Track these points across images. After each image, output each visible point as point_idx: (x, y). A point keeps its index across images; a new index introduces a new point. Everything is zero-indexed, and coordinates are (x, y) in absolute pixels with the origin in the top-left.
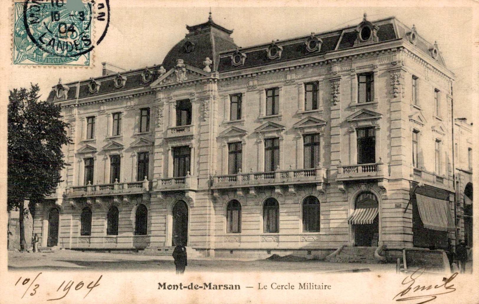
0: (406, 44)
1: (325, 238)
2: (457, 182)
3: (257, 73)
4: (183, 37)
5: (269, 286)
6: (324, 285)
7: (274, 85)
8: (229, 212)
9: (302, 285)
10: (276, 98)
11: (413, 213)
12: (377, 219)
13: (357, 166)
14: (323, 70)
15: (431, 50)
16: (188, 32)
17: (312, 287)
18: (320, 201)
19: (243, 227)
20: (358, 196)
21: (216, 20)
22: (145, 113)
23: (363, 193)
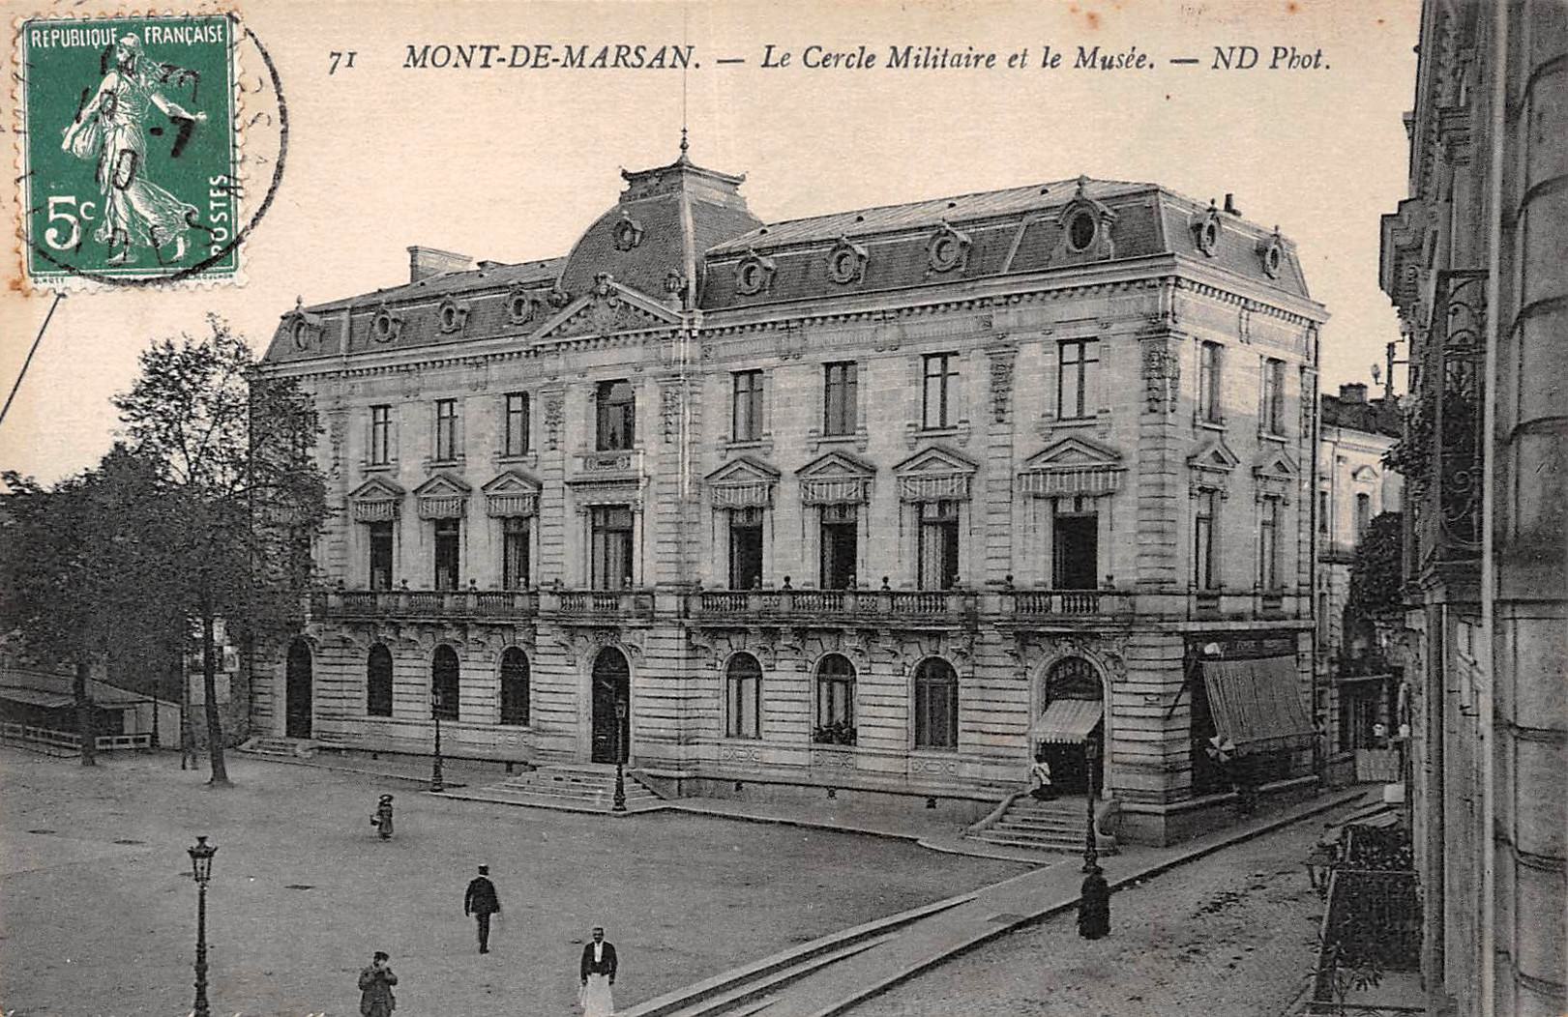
0: (1188, 266)
1: (967, 771)
2: (1323, 494)
3: (802, 320)
4: (613, 201)
5: (796, 59)
6: (973, 54)
7: (844, 356)
8: (733, 683)
9: (901, 51)
10: (849, 389)
11: (1193, 714)
12: (1098, 731)
13: (1050, 594)
14: (968, 321)
15: (1261, 252)
16: (625, 186)
17: (931, 62)
18: (959, 672)
19: (765, 726)
20: (1054, 669)
21: (695, 158)
22: (516, 403)
23: (1063, 661)
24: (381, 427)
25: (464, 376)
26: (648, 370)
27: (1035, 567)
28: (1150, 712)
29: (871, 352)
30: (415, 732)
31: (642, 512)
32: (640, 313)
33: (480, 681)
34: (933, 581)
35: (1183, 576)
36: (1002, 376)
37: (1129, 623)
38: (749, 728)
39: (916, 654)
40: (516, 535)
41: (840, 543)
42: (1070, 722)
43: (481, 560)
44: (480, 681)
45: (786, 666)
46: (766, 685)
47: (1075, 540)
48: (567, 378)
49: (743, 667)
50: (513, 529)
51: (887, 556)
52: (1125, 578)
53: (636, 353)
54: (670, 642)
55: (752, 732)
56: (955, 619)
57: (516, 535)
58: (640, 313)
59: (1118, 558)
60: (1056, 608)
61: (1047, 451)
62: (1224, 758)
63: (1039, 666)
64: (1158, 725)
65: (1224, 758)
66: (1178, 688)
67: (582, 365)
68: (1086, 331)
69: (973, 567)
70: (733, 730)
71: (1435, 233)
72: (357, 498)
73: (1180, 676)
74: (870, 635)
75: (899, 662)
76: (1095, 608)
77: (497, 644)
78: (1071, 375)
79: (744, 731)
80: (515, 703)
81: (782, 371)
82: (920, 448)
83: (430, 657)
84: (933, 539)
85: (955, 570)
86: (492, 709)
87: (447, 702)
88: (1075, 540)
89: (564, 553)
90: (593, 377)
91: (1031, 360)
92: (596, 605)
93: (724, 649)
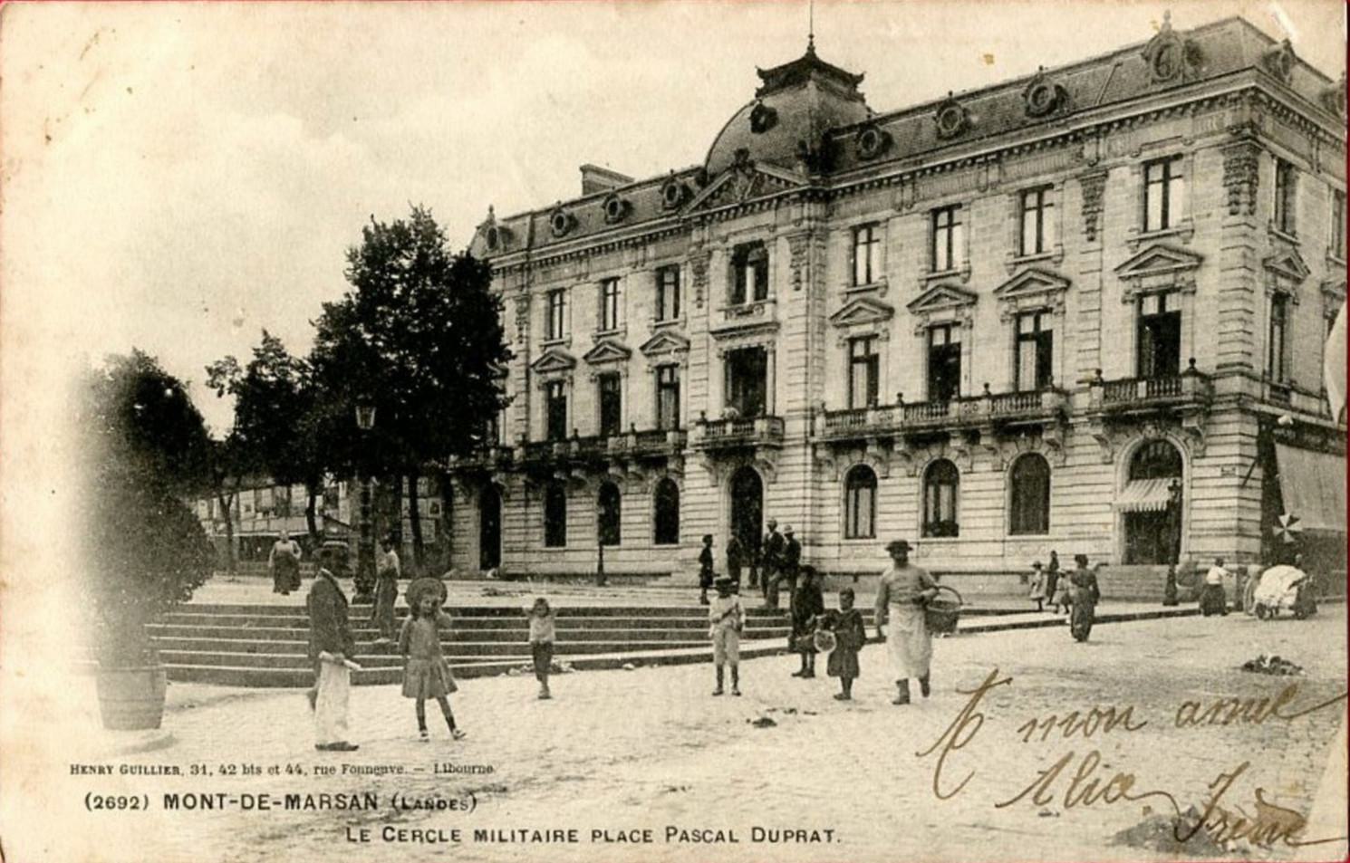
14: (1062, 157)
19: (879, 526)
24: (557, 309)
25: (484, 758)
26: (780, 230)
27: (1120, 362)
28: (1227, 481)
29: (974, 193)
30: (586, 556)
31: (774, 352)
32: (774, 181)
33: (637, 511)
34: (1028, 381)
35: (1259, 367)
36: (1093, 200)
37: (1207, 406)
38: (864, 527)
39: (1012, 451)
40: (668, 387)
41: (943, 367)
42: (1154, 495)
43: (638, 406)
44: (637, 511)
45: (898, 472)
46: (880, 491)
47: (1160, 336)
48: (712, 245)
49: (861, 479)
50: (666, 378)
51: (988, 366)
52: (1206, 364)
53: (768, 218)
54: (797, 461)
55: (868, 533)
56: (1049, 412)
57: (668, 387)
58: (774, 181)
59: (1202, 345)
60: (1142, 393)
61: (1133, 260)
62: (1288, 538)
63: (1127, 444)
64: (1235, 493)
65: (1288, 538)
66: (1251, 462)
67: (724, 233)
68: (1169, 150)
69: (1066, 370)
70: (851, 533)
71: (1097, 781)
72: (538, 368)
73: (1254, 451)
74: (972, 436)
75: (998, 459)
76: (1178, 390)
77: (653, 478)
78: (1155, 192)
79: (860, 532)
80: (666, 528)
81: (897, 219)
82: (1018, 272)
83: (595, 493)
84: (1029, 351)
85: (1049, 372)
86: (648, 530)
87: (609, 530)
88: (1160, 336)
89: (705, 395)
90: (733, 241)
91: (1123, 182)
92: (734, 430)
93: (847, 462)
